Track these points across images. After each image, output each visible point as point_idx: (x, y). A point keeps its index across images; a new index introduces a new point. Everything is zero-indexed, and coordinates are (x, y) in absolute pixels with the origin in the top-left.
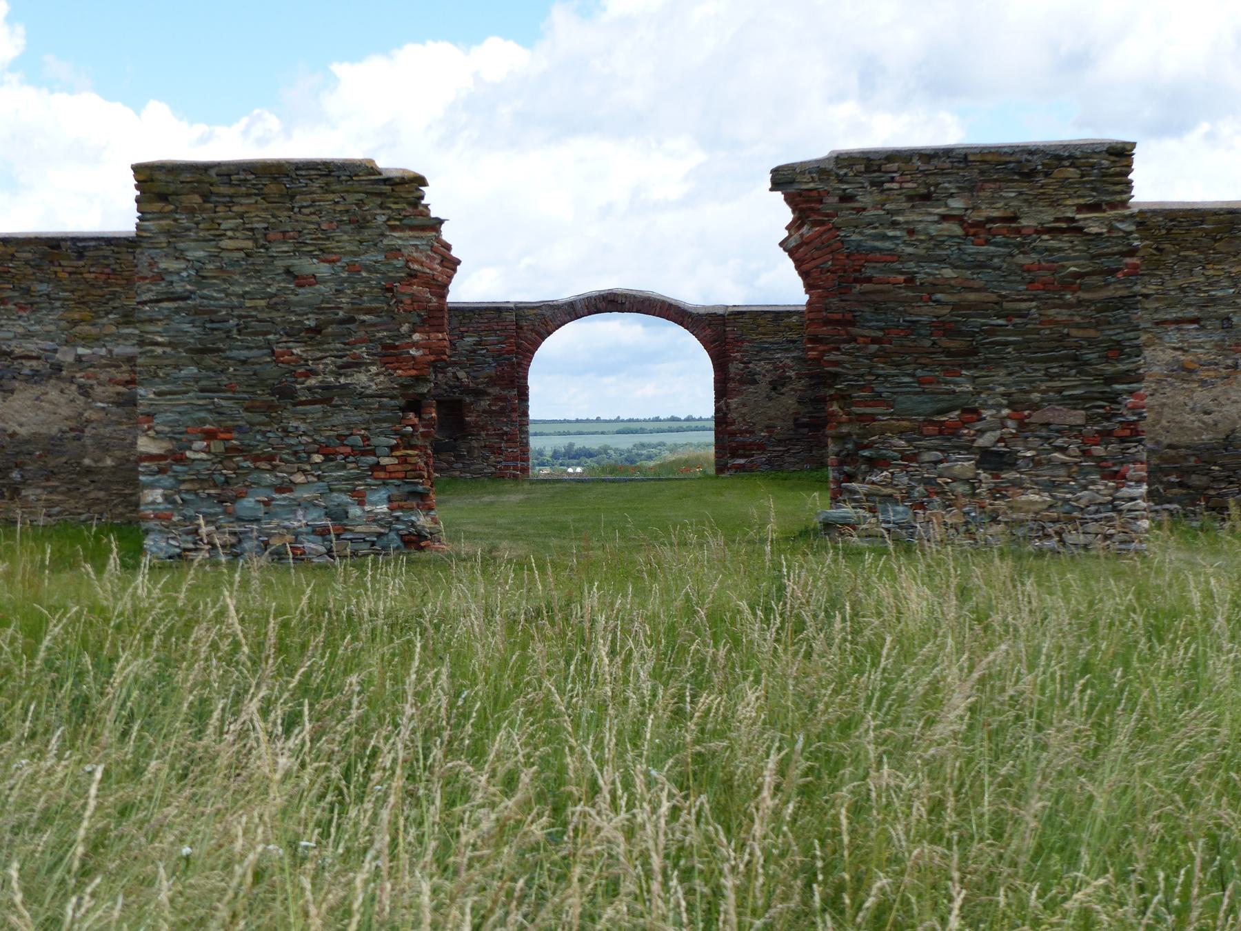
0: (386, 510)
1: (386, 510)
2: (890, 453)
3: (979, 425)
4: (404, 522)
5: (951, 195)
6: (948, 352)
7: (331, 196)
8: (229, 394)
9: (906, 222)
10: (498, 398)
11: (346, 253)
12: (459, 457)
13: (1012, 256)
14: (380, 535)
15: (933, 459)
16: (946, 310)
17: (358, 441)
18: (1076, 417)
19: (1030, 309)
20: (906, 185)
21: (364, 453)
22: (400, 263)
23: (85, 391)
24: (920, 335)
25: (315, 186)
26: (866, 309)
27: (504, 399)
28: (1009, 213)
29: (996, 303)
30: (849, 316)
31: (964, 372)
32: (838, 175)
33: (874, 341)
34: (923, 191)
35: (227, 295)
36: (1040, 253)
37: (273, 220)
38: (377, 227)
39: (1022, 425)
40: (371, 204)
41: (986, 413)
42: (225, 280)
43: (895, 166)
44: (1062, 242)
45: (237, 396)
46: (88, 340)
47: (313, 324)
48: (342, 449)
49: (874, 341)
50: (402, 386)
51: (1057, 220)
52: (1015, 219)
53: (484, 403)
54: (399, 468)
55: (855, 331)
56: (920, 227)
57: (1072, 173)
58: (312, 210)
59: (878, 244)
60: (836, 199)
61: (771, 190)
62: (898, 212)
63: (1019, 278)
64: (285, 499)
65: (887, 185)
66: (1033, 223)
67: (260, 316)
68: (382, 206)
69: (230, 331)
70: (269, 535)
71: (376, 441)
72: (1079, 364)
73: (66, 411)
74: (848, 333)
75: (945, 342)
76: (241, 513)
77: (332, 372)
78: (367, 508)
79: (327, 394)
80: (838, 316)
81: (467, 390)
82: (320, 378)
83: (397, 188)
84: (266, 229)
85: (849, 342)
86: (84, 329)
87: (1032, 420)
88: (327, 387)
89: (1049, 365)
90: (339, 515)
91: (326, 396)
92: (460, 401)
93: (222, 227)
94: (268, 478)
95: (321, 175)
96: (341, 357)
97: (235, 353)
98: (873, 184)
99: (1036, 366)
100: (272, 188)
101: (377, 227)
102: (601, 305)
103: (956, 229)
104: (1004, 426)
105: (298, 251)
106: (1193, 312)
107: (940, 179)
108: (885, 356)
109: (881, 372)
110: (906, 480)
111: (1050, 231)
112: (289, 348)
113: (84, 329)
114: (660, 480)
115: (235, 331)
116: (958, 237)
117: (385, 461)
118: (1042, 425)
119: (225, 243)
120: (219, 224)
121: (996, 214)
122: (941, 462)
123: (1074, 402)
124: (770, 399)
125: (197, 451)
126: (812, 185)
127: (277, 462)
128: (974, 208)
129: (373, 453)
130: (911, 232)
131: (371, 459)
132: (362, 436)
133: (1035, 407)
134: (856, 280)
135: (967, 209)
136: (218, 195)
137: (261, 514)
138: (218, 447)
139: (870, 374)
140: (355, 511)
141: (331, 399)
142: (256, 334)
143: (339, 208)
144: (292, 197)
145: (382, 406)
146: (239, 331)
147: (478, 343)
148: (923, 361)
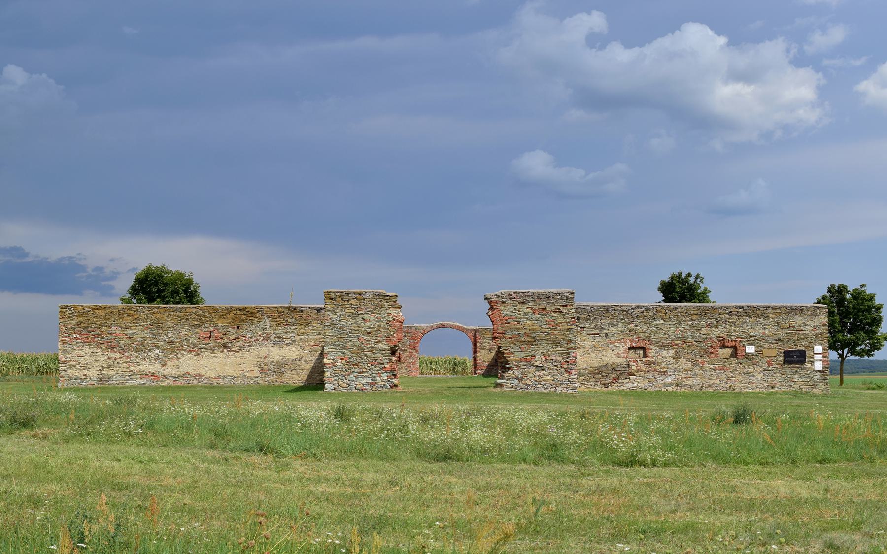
18: (560, 358)
23: (302, 347)
39: (546, 360)
44: (557, 315)
46: (303, 334)
53: (406, 353)
57: (559, 297)
72: (561, 345)
73: (297, 353)
86: (302, 331)
90: (374, 379)
91: (372, 350)
94: (357, 370)
100: (359, 297)
105: (366, 313)
106: (598, 332)
108: (512, 342)
113: (302, 331)
114: (475, 352)
123: (559, 354)
125: (339, 363)
138: (344, 362)
140: (378, 378)
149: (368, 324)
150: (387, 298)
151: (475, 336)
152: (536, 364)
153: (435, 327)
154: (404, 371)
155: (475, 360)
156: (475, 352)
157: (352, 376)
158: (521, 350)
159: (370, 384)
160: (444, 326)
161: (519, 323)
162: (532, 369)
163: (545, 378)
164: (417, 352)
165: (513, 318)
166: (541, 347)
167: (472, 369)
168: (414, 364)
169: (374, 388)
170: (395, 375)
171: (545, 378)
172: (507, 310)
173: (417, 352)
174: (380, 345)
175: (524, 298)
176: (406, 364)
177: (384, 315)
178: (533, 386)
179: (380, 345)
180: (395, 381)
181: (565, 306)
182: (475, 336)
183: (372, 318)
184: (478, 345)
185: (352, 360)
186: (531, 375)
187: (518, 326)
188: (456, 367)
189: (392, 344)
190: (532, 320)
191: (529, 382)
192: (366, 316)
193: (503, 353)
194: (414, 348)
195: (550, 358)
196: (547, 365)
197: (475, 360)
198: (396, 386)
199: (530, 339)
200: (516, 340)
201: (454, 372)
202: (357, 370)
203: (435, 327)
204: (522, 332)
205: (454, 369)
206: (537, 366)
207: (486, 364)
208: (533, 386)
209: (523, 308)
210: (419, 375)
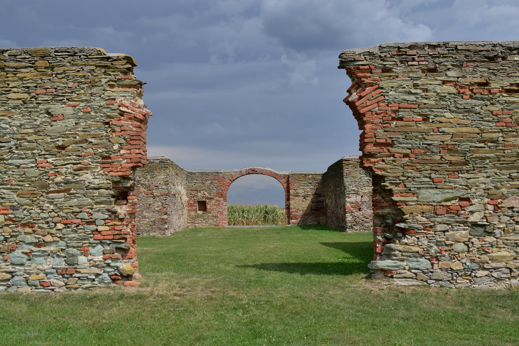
0: (101, 259)
1: (101, 259)
2: (416, 225)
3: (471, 208)
4: (112, 267)
5: (449, 69)
6: (451, 163)
7: (74, 68)
8: (9, 186)
9: (423, 85)
10: (217, 201)
11: (82, 101)
12: (204, 219)
13: (486, 106)
14: (98, 275)
15: (443, 229)
16: (449, 137)
17: (86, 216)
19: (498, 137)
20: (421, 63)
21: (89, 223)
22: (115, 107)
24: (433, 152)
25: (65, 62)
26: (400, 137)
27: (219, 201)
28: (483, 80)
29: (478, 134)
30: (389, 141)
31: (460, 175)
32: (380, 57)
33: (406, 156)
34: (432, 66)
35: (11, 126)
36: (502, 104)
37: (40, 81)
38: (102, 86)
39: (497, 208)
40: (99, 71)
41: (474, 201)
42: (10, 117)
43: (414, 52)
45: (13, 187)
47: (60, 143)
48: (75, 221)
49: (406, 156)
50: (114, 182)
51: (511, 85)
52: (487, 84)
54: (110, 232)
55: (393, 150)
56: (430, 87)
58: (63, 75)
59: (407, 97)
60: (380, 71)
61: (339, 68)
62: (419, 78)
63: (491, 119)
64: (39, 251)
65: (410, 63)
66: (498, 86)
67: (29, 138)
68: (105, 73)
69: (11, 148)
70: (29, 274)
71: (96, 215)
74: (389, 150)
75: (448, 157)
76: (14, 260)
77: (71, 173)
78: (90, 257)
79: (67, 187)
80: (383, 141)
81: (208, 198)
82: (63, 177)
83: (114, 63)
84: (36, 87)
85: (390, 156)
87: (502, 205)
88: (67, 182)
89: (511, 171)
90: (71, 262)
92: (205, 202)
93: (10, 86)
94: (30, 238)
95: (70, 55)
96: (77, 164)
97: (14, 161)
98: (401, 62)
99: (503, 171)
100: (40, 63)
101: (102, 86)
102: (250, 172)
103: (453, 90)
104: (486, 209)
105: (56, 98)
107: (441, 60)
108: (411, 165)
109: (410, 175)
110: (426, 242)
111: (508, 91)
112: (46, 158)
114: (288, 199)
115: (14, 147)
116: (454, 94)
117: (100, 228)
118: (509, 208)
119: (11, 95)
120: (9, 84)
121: (476, 80)
122: (448, 231)
124: (303, 201)
126: (365, 62)
127: (35, 229)
128: (463, 77)
129: (93, 223)
130: (426, 90)
131: (93, 227)
132: (88, 213)
133: (504, 197)
134: (393, 119)
135: (458, 78)
136: (9, 67)
137: (24, 261)
139: (403, 176)
140: (82, 259)
141: (70, 190)
142: (27, 149)
143: (79, 74)
144: (52, 68)
145: (100, 195)
146: (17, 148)
147: (212, 183)
148: (435, 168)
149: (59, 125)
150: (106, 63)
151: (288, 183)
152: (473, 218)
153: (244, 173)
154: (211, 221)
155: (288, 208)
156: (288, 199)
157: (18, 252)
158: (435, 185)
159: (63, 273)
160: (254, 172)
161: (426, 119)
162: (462, 233)
163: (495, 253)
164: (225, 200)
165: (411, 107)
166: (481, 178)
167: (284, 217)
168: (221, 214)
169: (72, 282)
170: (124, 251)
171: (495, 253)
172: (397, 87)
173: (225, 200)
174: (87, 177)
175: (434, 58)
176: (214, 213)
177: (98, 102)
178: (468, 273)
179: (87, 177)
180: (125, 266)
181: (55, 121)
182: (288, 183)
183: (69, 111)
184: (291, 192)
185: (20, 214)
186: (460, 247)
187: (423, 127)
188: (267, 216)
189: (116, 175)
190: (457, 110)
191: (456, 266)
192: (57, 108)
193: (391, 192)
194: (222, 196)
195: (506, 203)
196: (499, 222)
197: (288, 208)
198: (129, 277)
199: (455, 159)
200: (420, 158)
201: (265, 220)
202: (30, 238)
203: (244, 173)
204: (435, 139)
205: (265, 217)
206: (475, 225)
207: (300, 213)
208: (468, 273)
209: (434, 83)
210: (227, 226)
